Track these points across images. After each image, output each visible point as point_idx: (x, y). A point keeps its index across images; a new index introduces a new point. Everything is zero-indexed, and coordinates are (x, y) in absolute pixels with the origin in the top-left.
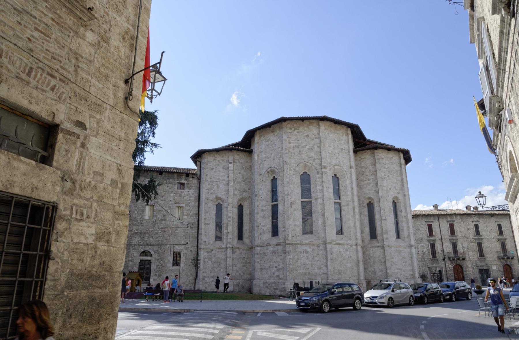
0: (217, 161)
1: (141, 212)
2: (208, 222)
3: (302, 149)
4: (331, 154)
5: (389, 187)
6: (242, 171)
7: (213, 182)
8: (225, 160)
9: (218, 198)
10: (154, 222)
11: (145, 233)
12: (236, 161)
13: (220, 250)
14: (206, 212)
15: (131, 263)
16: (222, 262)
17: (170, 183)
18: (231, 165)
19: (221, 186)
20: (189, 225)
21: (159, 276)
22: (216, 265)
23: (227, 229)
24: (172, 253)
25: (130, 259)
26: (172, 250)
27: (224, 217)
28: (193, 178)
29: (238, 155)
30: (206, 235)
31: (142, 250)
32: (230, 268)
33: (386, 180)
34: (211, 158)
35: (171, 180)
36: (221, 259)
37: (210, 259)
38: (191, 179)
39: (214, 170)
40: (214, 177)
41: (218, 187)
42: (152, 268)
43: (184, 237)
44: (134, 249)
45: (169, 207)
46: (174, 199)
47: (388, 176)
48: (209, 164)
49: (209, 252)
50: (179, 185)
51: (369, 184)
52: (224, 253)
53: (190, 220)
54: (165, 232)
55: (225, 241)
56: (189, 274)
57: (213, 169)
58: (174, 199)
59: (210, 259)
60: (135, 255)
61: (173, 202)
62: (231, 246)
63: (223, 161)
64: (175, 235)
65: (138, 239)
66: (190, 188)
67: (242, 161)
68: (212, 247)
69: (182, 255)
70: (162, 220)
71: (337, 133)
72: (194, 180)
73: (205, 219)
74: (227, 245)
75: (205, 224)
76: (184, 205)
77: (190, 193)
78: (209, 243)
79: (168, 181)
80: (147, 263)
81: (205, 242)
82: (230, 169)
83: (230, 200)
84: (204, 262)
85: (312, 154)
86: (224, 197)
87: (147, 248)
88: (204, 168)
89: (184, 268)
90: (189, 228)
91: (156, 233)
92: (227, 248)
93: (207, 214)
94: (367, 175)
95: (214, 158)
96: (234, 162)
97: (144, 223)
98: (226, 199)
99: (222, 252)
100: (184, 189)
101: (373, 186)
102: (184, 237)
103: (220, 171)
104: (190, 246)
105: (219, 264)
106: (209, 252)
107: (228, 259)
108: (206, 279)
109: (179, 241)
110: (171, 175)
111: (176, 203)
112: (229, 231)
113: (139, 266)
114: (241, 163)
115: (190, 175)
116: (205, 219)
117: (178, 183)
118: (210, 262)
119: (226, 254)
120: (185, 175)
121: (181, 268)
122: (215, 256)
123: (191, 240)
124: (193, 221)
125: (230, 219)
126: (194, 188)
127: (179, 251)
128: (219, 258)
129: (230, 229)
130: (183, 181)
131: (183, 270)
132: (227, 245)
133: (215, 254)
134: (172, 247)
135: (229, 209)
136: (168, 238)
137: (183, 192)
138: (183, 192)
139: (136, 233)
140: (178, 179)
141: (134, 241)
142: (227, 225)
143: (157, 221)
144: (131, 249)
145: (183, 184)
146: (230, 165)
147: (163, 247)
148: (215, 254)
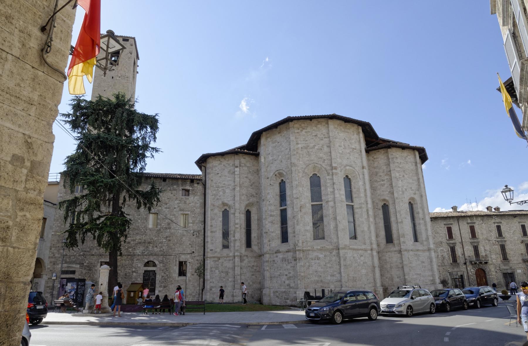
0: (222, 165)
1: (145, 221)
3: (311, 150)
4: (342, 154)
5: (405, 187)
6: (250, 176)
8: (231, 165)
9: (224, 204)
10: (158, 231)
11: (149, 243)
12: (242, 165)
13: (228, 259)
14: (212, 219)
15: (134, 274)
16: (230, 271)
17: (174, 190)
18: (237, 169)
19: (228, 191)
21: (165, 287)
22: (223, 275)
23: (234, 237)
25: (134, 270)
26: (178, 260)
27: (231, 224)
28: (198, 183)
29: (244, 158)
31: (146, 261)
32: (239, 277)
33: (402, 181)
34: (217, 162)
35: (175, 187)
36: (229, 268)
37: (217, 268)
38: (196, 185)
39: (220, 175)
41: (224, 192)
43: (190, 246)
44: (138, 260)
45: (174, 215)
48: (214, 169)
50: (184, 191)
52: (231, 262)
53: (196, 228)
54: (169, 240)
55: (232, 249)
56: (196, 284)
57: (218, 174)
58: (179, 206)
59: (217, 268)
60: (139, 265)
61: (178, 209)
62: (238, 254)
63: (229, 165)
64: (180, 244)
66: (195, 195)
67: (248, 165)
68: (219, 255)
69: (188, 264)
70: (166, 228)
71: (348, 132)
72: (199, 186)
74: (234, 253)
75: (212, 232)
76: (189, 213)
77: (195, 200)
78: (216, 252)
79: (172, 188)
80: (151, 274)
81: (211, 250)
82: (236, 173)
83: (237, 206)
84: (211, 271)
86: (231, 203)
87: (151, 259)
88: (209, 174)
89: (190, 279)
90: (195, 236)
91: (161, 243)
92: (234, 257)
94: (380, 176)
95: (219, 162)
96: (240, 166)
97: (148, 232)
98: (233, 204)
99: (230, 260)
100: (189, 195)
101: (387, 187)
102: (190, 246)
103: (225, 176)
104: (196, 254)
105: (227, 273)
106: (216, 261)
108: (213, 289)
110: (175, 181)
111: (181, 210)
113: (144, 277)
114: (248, 167)
115: (195, 181)
116: (211, 226)
117: (183, 189)
118: (217, 271)
119: (234, 263)
120: (189, 181)
121: (187, 278)
122: (222, 265)
123: (197, 248)
124: (199, 229)
125: (237, 226)
126: (199, 194)
127: (184, 260)
128: (226, 267)
129: (237, 236)
130: (188, 187)
131: (190, 281)
132: (234, 253)
133: (223, 262)
134: (178, 256)
136: (174, 247)
137: (188, 199)
138: (188, 199)
139: (140, 243)
141: (138, 251)
142: (234, 232)
143: (162, 230)
144: (135, 259)
145: (188, 191)
146: (236, 169)
147: (168, 257)
148: (223, 262)
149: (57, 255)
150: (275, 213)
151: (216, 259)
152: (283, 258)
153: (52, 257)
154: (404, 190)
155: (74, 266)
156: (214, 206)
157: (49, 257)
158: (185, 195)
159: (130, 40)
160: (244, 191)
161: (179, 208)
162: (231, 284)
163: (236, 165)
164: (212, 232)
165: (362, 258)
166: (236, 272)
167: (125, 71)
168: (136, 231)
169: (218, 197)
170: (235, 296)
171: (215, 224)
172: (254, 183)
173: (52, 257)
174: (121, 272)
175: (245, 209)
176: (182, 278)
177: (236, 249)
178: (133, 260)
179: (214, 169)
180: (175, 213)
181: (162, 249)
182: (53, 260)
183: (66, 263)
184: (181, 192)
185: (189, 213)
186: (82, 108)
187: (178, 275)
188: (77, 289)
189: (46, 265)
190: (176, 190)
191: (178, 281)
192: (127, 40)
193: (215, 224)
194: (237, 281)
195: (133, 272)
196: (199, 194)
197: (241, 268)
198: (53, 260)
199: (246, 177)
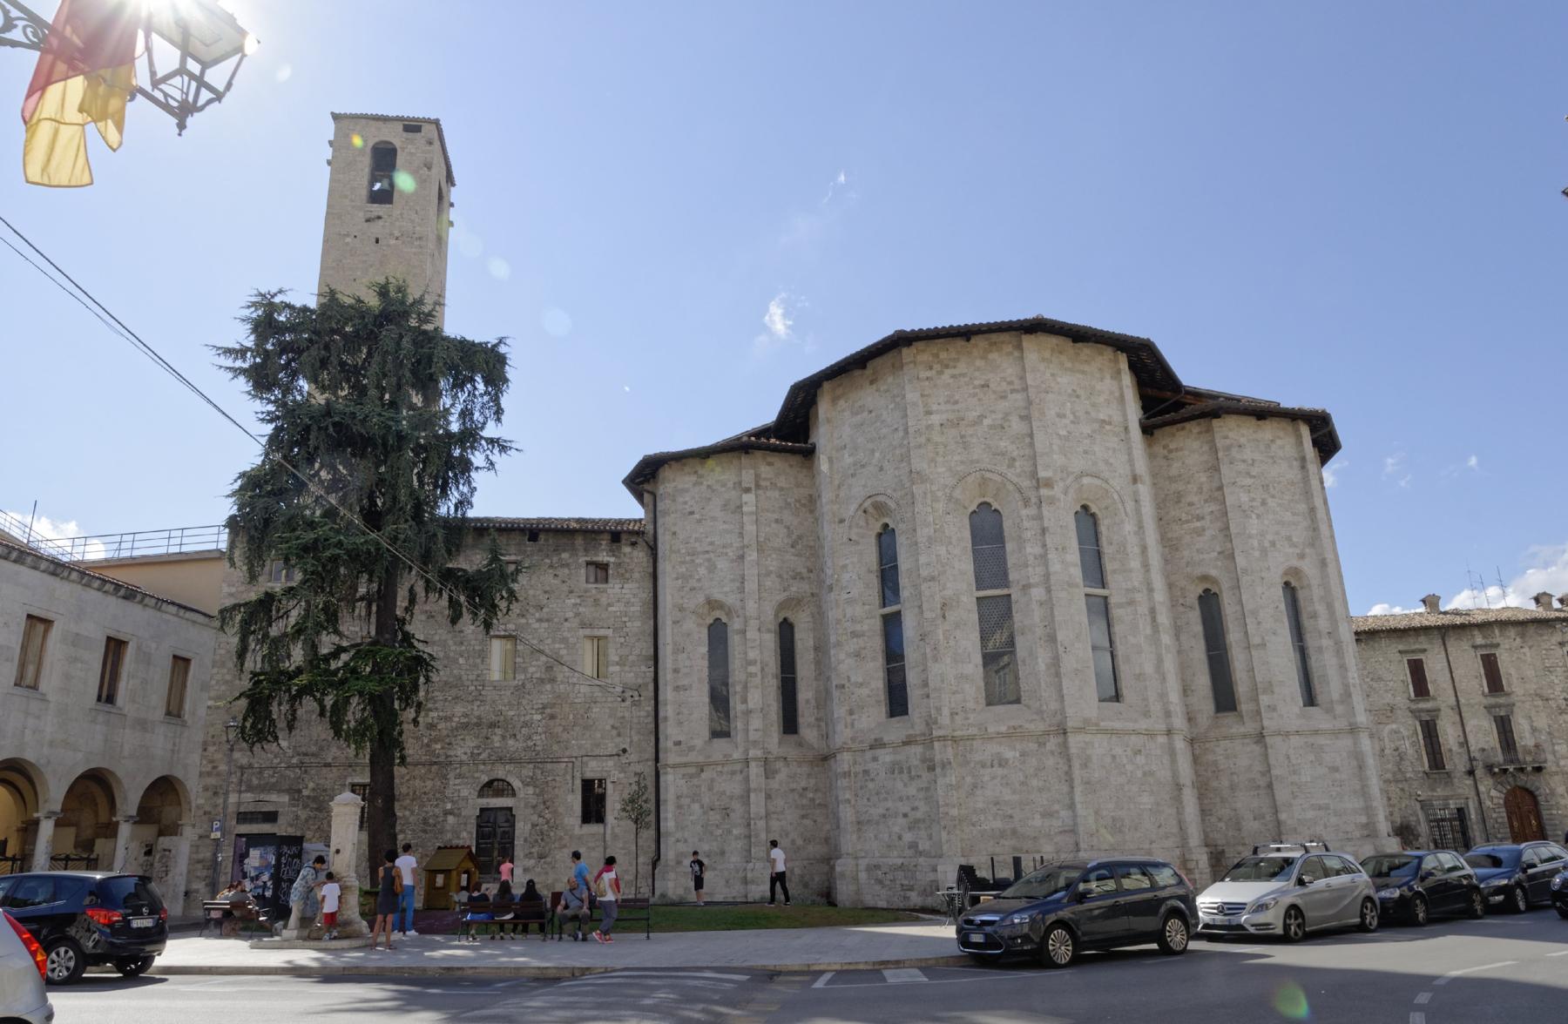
2: (686, 682)
3: (970, 431)
4: (1067, 438)
5: (1270, 537)
6: (787, 517)
7: (693, 553)
8: (730, 484)
9: (712, 604)
10: (517, 688)
11: (493, 725)
12: (763, 483)
14: (679, 650)
15: (451, 819)
16: (737, 805)
17: (563, 566)
18: (749, 498)
19: (722, 564)
20: (628, 694)
21: (541, 857)
22: (715, 817)
23: (745, 701)
24: (578, 783)
25: (449, 806)
26: (578, 775)
28: (634, 544)
29: (770, 464)
30: (680, 723)
32: (761, 824)
33: (1258, 516)
34: (687, 478)
35: (565, 555)
36: (731, 798)
37: (695, 798)
38: (627, 549)
39: (697, 516)
40: (697, 540)
41: (712, 568)
42: (517, 833)
43: (614, 732)
44: (459, 776)
45: (564, 640)
46: (577, 615)
47: (1264, 503)
48: (681, 500)
49: (691, 776)
50: (592, 568)
51: (1200, 532)
52: (739, 777)
53: (630, 677)
54: (552, 717)
55: (739, 738)
57: (692, 513)
58: (577, 615)
59: (695, 798)
60: (464, 793)
61: (575, 623)
62: (759, 753)
64: (586, 728)
65: (471, 743)
66: (624, 579)
68: (701, 759)
69: (610, 787)
70: (542, 681)
71: (1083, 372)
72: (635, 553)
73: (676, 671)
74: (746, 751)
75: (677, 688)
76: (609, 632)
77: (625, 594)
78: (691, 749)
79: (555, 559)
80: (501, 819)
81: (678, 743)
82: (745, 509)
83: (751, 607)
84: (679, 807)
85: (1003, 444)
86: (731, 600)
87: (500, 772)
88: (666, 513)
89: (617, 830)
90: (628, 703)
91: (526, 724)
92: (747, 762)
93: (682, 656)
94: (1191, 504)
95: (694, 478)
96: (758, 486)
97: (489, 693)
98: (738, 603)
99: (733, 773)
101: (1214, 537)
102: (614, 732)
103: (714, 519)
104: (633, 757)
105: (726, 812)
106: (691, 776)
107: (752, 795)
109: (598, 745)
111: (583, 626)
112: (751, 705)
113: (479, 826)
114: (782, 489)
115: (624, 537)
116: (676, 671)
117: (588, 564)
118: (696, 806)
119: (747, 780)
120: (607, 536)
121: (609, 832)
122: (710, 789)
123: (635, 738)
124: (640, 681)
125: (752, 669)
126: (636, 575)
128: (724, 793)
129: (755, 699)
130: (603, 557)
131: (615, 837)
132: (746, 751)
134: (578, 763)
135: (749, 635)
136: (565, 736)
137: (605, 591)
138: (605, 591)
139: (465, 726)
140: (586, 550)
141: (459, 752)
142: (745, 687)
143: (528, 686)
144: (452, 775)
145: (603, 567)
146: (746, 497)
147: (549, 766)
148: (712, 780)
149: (223, 768)
150: (865, 627)
151: (692, 770)
152: (894, 763)
153: (209, 774)
154: (1267, 544)
155: (274, 797)
156: (681, 609)
157: (201, 774)
158: (596, 581)
159: (426, 127)
160: (772, 563)
161: (577, 620)
162: (740, 844)
163: (745, 485)
164: (677, 688)
165: (1140, 760)
166: (753, 809)
167: (412, 221)
168: (454, 692)
169: (693, 583)
170: (753, 882)
171: (687, 663)
172: (800, 537)
173: (209, 774)
174: (412, 813)
175: (776, 616)
176: (594, 828)
177: (751, 738)
178: (445, 777)
179: (681, 500)
180: (566, 634)
181: (530, 743)
182: (212, 781)
183: (250, 789)
184: (583, 571)
185: (609, 632)
186: (281, 329)
187: (579, 821)
188: (278, 865)
189: (193, 797)
190: (567, 565)
191: (580, 838)
192: (417, 129)
193: (687, 663)
194: (757, 836)
195: (447, 813)
196: (636, 575)
197: (768, 797)
198: (212, 781)
199: (777, 521)
